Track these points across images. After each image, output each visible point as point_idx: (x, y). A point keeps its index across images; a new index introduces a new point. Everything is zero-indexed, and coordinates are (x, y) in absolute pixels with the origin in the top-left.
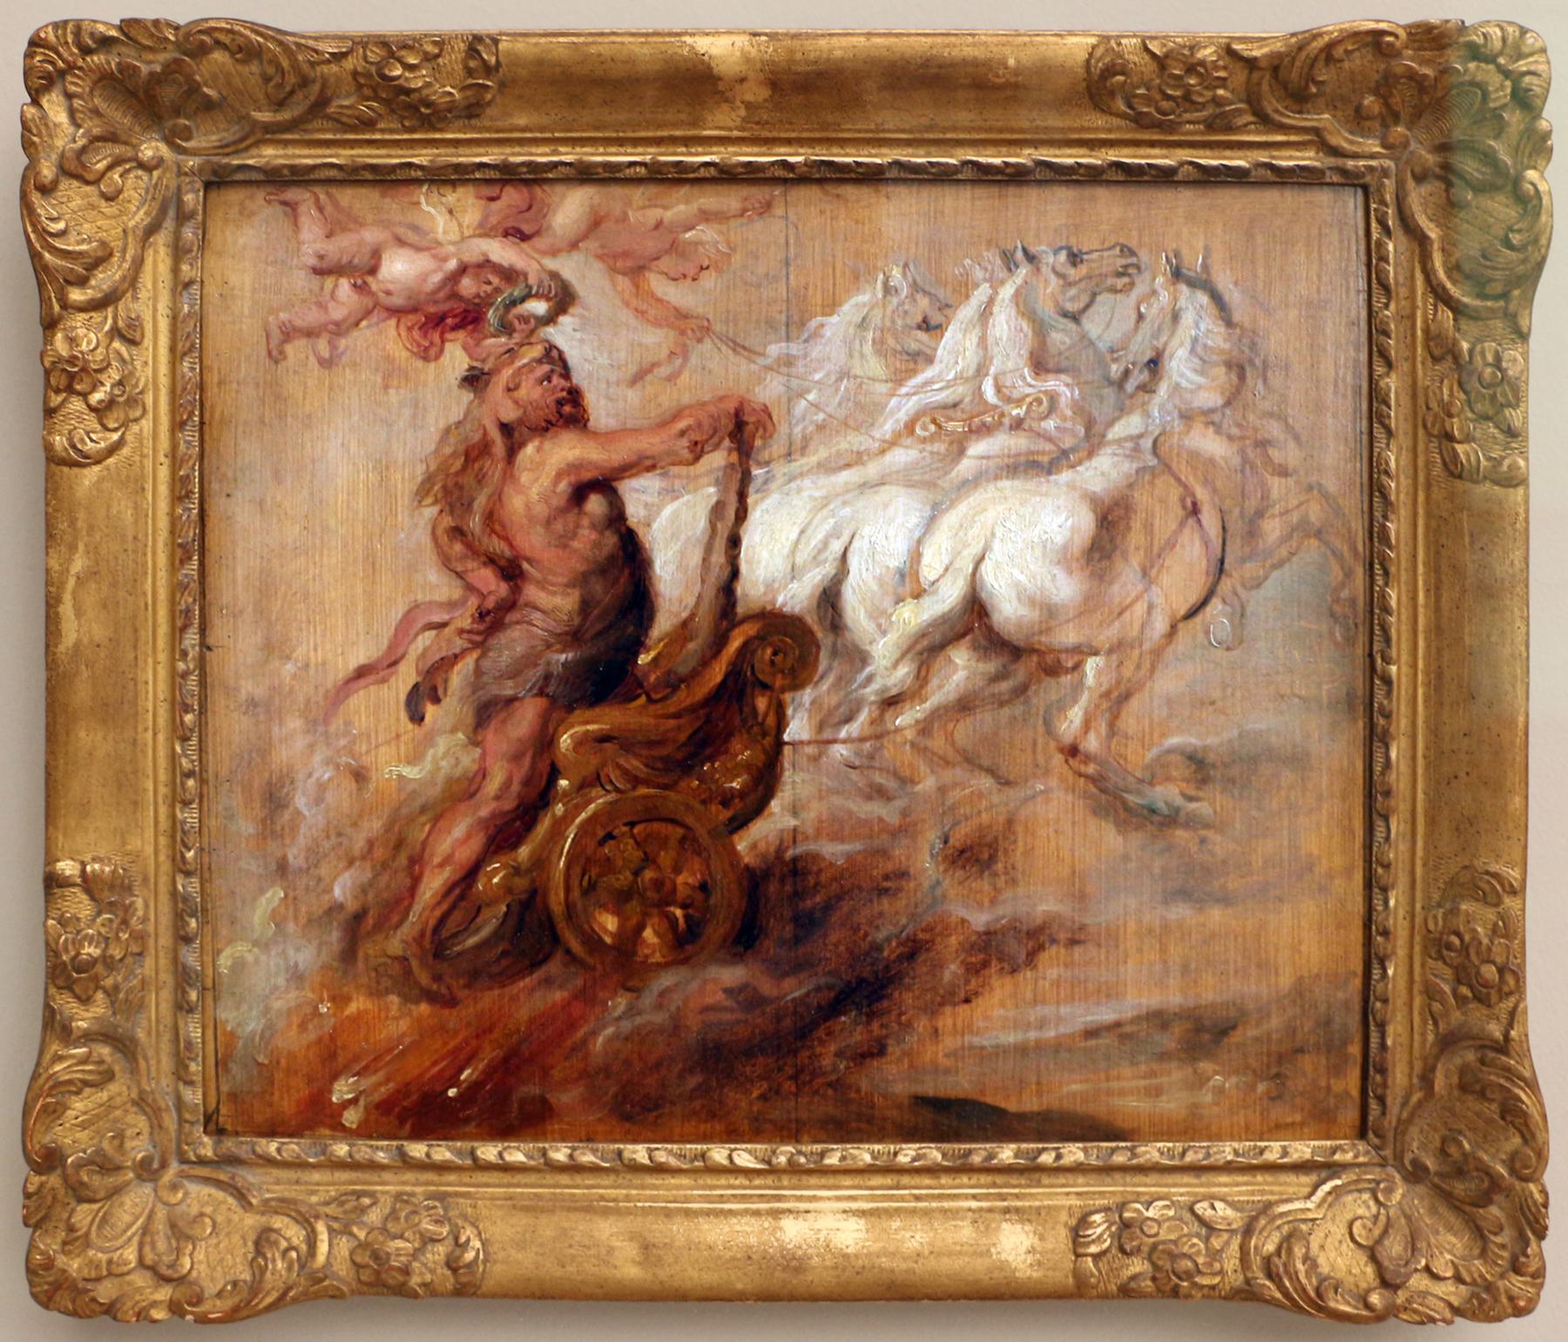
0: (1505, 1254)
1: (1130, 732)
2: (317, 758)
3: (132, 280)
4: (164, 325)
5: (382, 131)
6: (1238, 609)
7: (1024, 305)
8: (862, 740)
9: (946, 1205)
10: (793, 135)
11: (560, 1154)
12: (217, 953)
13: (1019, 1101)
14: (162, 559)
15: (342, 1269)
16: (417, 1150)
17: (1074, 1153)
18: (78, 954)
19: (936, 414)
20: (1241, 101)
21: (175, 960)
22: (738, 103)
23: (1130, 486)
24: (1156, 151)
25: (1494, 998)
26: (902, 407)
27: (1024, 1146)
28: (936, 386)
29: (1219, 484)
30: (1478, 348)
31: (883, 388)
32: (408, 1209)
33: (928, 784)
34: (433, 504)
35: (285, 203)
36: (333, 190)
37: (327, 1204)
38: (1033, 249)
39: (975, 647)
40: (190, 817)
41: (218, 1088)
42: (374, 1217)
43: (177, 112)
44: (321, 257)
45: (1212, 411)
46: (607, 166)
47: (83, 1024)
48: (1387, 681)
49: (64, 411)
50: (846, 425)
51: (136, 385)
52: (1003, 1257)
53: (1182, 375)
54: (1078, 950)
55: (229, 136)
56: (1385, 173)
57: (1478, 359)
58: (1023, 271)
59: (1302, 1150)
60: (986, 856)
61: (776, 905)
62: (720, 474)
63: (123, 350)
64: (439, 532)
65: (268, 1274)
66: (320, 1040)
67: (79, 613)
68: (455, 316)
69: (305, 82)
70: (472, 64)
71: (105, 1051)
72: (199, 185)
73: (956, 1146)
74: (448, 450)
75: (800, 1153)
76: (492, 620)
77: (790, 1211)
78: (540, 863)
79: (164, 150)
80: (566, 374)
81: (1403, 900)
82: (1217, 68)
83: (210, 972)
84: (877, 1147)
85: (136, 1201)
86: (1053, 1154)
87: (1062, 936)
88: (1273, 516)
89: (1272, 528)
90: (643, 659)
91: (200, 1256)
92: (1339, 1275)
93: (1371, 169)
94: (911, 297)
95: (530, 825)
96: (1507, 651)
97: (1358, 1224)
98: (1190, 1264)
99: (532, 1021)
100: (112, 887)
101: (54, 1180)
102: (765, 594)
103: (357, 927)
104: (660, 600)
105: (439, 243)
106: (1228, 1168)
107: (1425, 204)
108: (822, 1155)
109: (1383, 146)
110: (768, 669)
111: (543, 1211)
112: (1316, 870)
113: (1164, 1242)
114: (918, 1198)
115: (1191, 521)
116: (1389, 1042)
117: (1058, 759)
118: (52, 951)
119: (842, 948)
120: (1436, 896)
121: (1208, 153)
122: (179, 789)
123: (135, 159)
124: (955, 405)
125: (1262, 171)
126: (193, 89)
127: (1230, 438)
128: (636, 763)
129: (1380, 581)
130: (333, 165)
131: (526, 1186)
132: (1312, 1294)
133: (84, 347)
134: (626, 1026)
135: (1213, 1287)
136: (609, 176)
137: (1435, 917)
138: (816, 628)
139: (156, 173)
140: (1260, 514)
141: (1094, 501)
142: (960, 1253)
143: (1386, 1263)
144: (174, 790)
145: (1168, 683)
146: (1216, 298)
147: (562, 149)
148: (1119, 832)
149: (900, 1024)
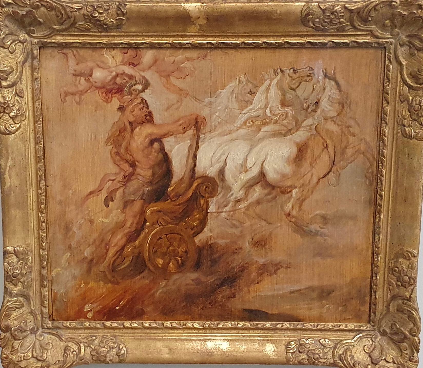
0: (407, 356)
1: (305, 209)
2: (79, 217)
3: (20, 78)
4: (30, 91)
5: (93, 32)
6: (338, 175)
7: (279, 86)
8: (230, 211)
9: (251, 338)
10: (213, 34)
11: (147, 325)
12: (51, 271)
13: (272, 310)
14: (33, 161)
15: (88, 356)
16: (108, 324)
17: (287, 325)
18: (14, 272)
19: (253, 119)
20: (348, 22)
21: (40, 274)
22: (197, 25)
23: (308, 140)
24: (321, 38)
25: (407, 286)
26: (243, 117)
27: (273, 323)
28: (253, 111)
29: (334, 139)
30: (414, 99)
31: (238, 111)
32: (106, 340)
33: (248, 223)
34: (111, 144)
35: (63, 53)
36: (78, 50)
37: (84, 339)
38: (283, 69)
39: (262, 186)
40: (43, 234)
41: (52, 308)
42: (96, 342)
43: (30, 25)
44: (75, 71)
45: (334, 117)
46: (159, 44)
47: (16, 292)
48: (381, 196)
49: (2, 118)
50: (227, 123)
51: (23, 110)
52: (266, 353)
53: (325, 107)
54: (289, 269)
55: (46, 33)
56: (391, 44)
57: (414, 102)
58: (280, 75)
59: (351, 326)
60: (264, 244)
61: (205, 257)
62: (191, 137)
63: (19, 99)
64: (112, 153)
65: (68, 359)
66: (81, 295)
67: (10, 177)
68: (115, 90)
69: (69, 17)
70: (119, 12)
71: (22, 299)
72: (38, 48)
73: (254, 322)
74: (114, 130)
75: (212, 324)
76: (128, 178)
77: (209, 339)
78: (141, 245)
79: (27, 36)
80: (148, 107)
81: (383, 257)
82: (341, 13)
83: (50, 276)
84: (233, 322)
85: (30, 339)
86: (281, 325)
87: (285, 266)
88: (350, 148)
89: (349, 152)
90: (170, 189)
91: (49, 354)
92: (360, 360)
93: (387, 42)
94: (246, 84)
95: (139, 235)
96: (416, 188)
97: (366, 346)
98: (318, 356)
99: (139, 288)
100: (22, 254)
101: (8, 334)
102: (203, 171)
103: (91, 263)
104: (174, 172)
105: (110, 67)
106: (330, 330)
107: (402, 54)
108: (218, 324)
109: (391, 35)
110: (204, 192)
111: (142, 340)
112: (358, 248)
113: (312, 350)
114: (244, 336)
115: (325, 150)
116: (377, 297)
117: (284, 217)
118: (6, 272)
119: (224, 268)
120: (392, 257)
121: (337, 38)
122: (41, 226)
123: (18, 40)
124: (258, 116)
125: (354, 44)
126: (36, 19)
127: (338, 125)
128: (167, 218)
129: (381, 167)
130: (78, 42)
131: (138, 333)
132: (352, 365)
133: (7, 99)
134: (165, 289)
135: (324, 362)
136: (159, 47)
137: (392, 263)
138: (217, 181)
139: (24, 44)
140: (346, 147)
141: (297, 144)
142: (255, 352)
143: (373, 358)
144: (39, 225)
145: (316, 196)
146: (337, 83)
147: (146, 38)
148: (301, 237)
149: (239, 289)
